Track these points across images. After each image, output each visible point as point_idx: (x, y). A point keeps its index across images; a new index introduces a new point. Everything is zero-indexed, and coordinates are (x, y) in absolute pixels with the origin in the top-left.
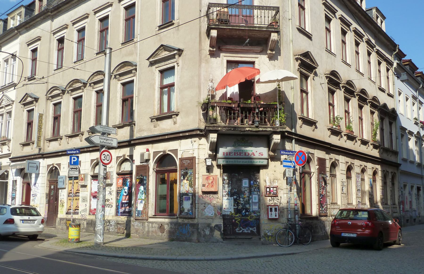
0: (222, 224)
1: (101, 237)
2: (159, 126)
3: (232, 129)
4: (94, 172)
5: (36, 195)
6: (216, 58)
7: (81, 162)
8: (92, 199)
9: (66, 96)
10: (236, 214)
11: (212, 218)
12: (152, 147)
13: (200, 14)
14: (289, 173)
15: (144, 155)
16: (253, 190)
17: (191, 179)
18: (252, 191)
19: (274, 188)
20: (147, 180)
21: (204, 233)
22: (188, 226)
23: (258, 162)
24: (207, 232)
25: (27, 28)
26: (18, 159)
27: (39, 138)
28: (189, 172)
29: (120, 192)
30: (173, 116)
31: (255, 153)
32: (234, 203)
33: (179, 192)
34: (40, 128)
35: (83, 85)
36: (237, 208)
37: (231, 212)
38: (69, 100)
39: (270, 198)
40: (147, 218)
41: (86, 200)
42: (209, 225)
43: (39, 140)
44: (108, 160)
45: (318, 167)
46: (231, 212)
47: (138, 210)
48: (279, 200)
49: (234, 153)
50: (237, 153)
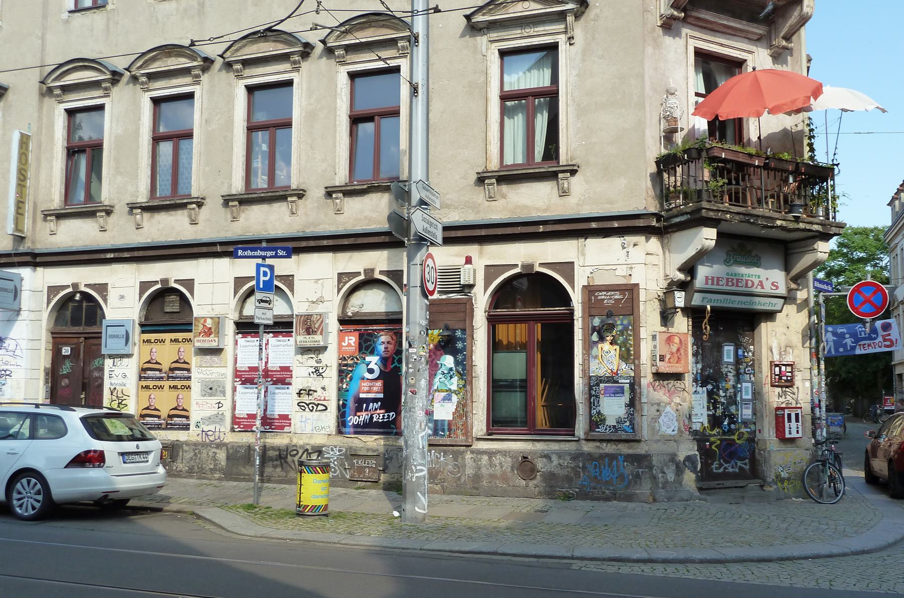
1: (425, 498)
2: (504, 196)
3: (752, 221)
4: (241, 312)
5: (8, 373)
6: (674, 39)
8: (240, 388)
10: (712, 429)
15: (462, 276)
16: (742, 371)
17: (626, 340)
18: (741, 374)
19: (787, 367)
20: (468, 341)
21: (663, 476)
22: (622, 463)
23: (762, 304)
24: (671, 476)
26: (126, 255)
27: (21, 205)
28: (619, 322)
29: (350, 369)
32: (709, 402)
33: (584, 371)
35: (202, 63)
36: (714, 415)
37: (703, 424)
38: (333, 82)
39: (779, 390)
40: (470, 440)
41: (221, 389)
43: (20, 211)
46: (703, 424)
47: (436, 421)
48: (794, 394)
49: (725, 279)
50: (733, 279)
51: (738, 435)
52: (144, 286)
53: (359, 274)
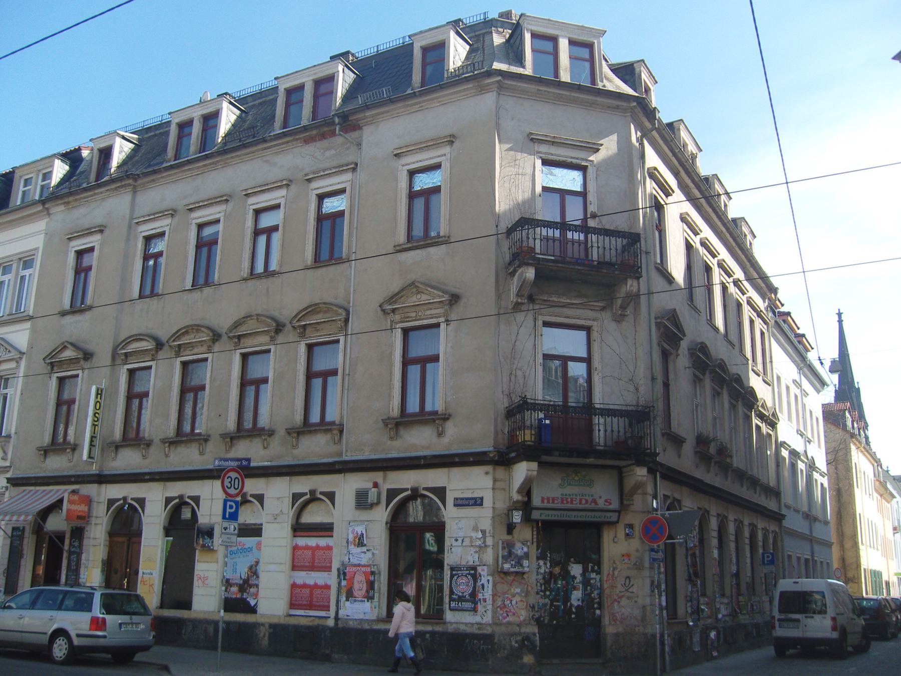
12: (385, 478)
25: (68, 203)
27: (93, 439)
30: (437, 422)
43: (93, 444)
44: (236, 487)
52: (168, 500)
53: (305, 494)
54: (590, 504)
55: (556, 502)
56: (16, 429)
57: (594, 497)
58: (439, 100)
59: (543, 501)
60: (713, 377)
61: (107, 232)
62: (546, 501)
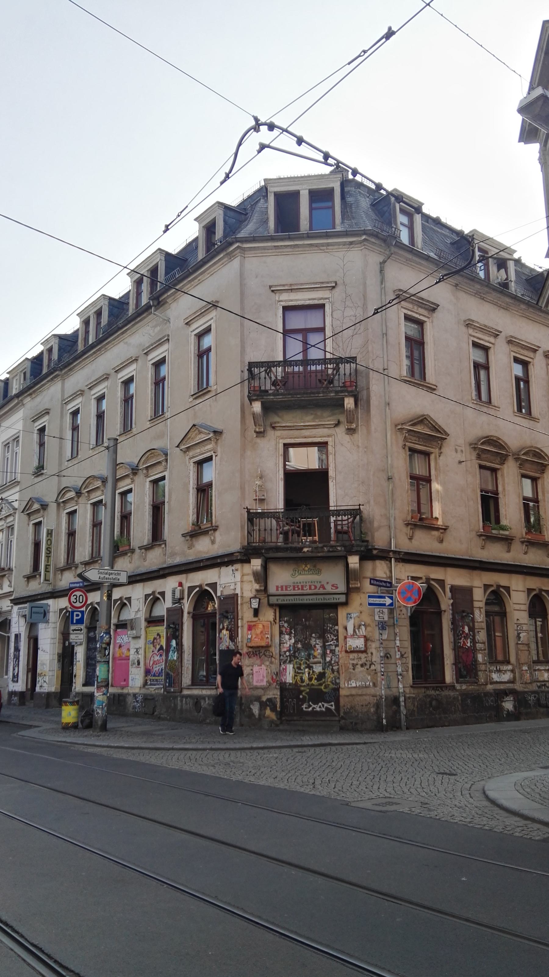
0: (278, 697)
4: (118, 618)
7: (132, 599)
9: (82, 500)
11: (264, 689)
13: (365, 307)
14: (381, 615)
20: (180, 630)
31: (326, 586)
34: (48, 552)
42: (258, 699)
43: (47, 570)
45: (452, 601)
51: (325, 686)
54: (319, 589)
55: (288, 589)
56: (15, 564)
57: (322, 584)
58: (208, 272)
59: (277, 590)
60: (520, 465)
61: (51, 412)
62: (280, 589)
